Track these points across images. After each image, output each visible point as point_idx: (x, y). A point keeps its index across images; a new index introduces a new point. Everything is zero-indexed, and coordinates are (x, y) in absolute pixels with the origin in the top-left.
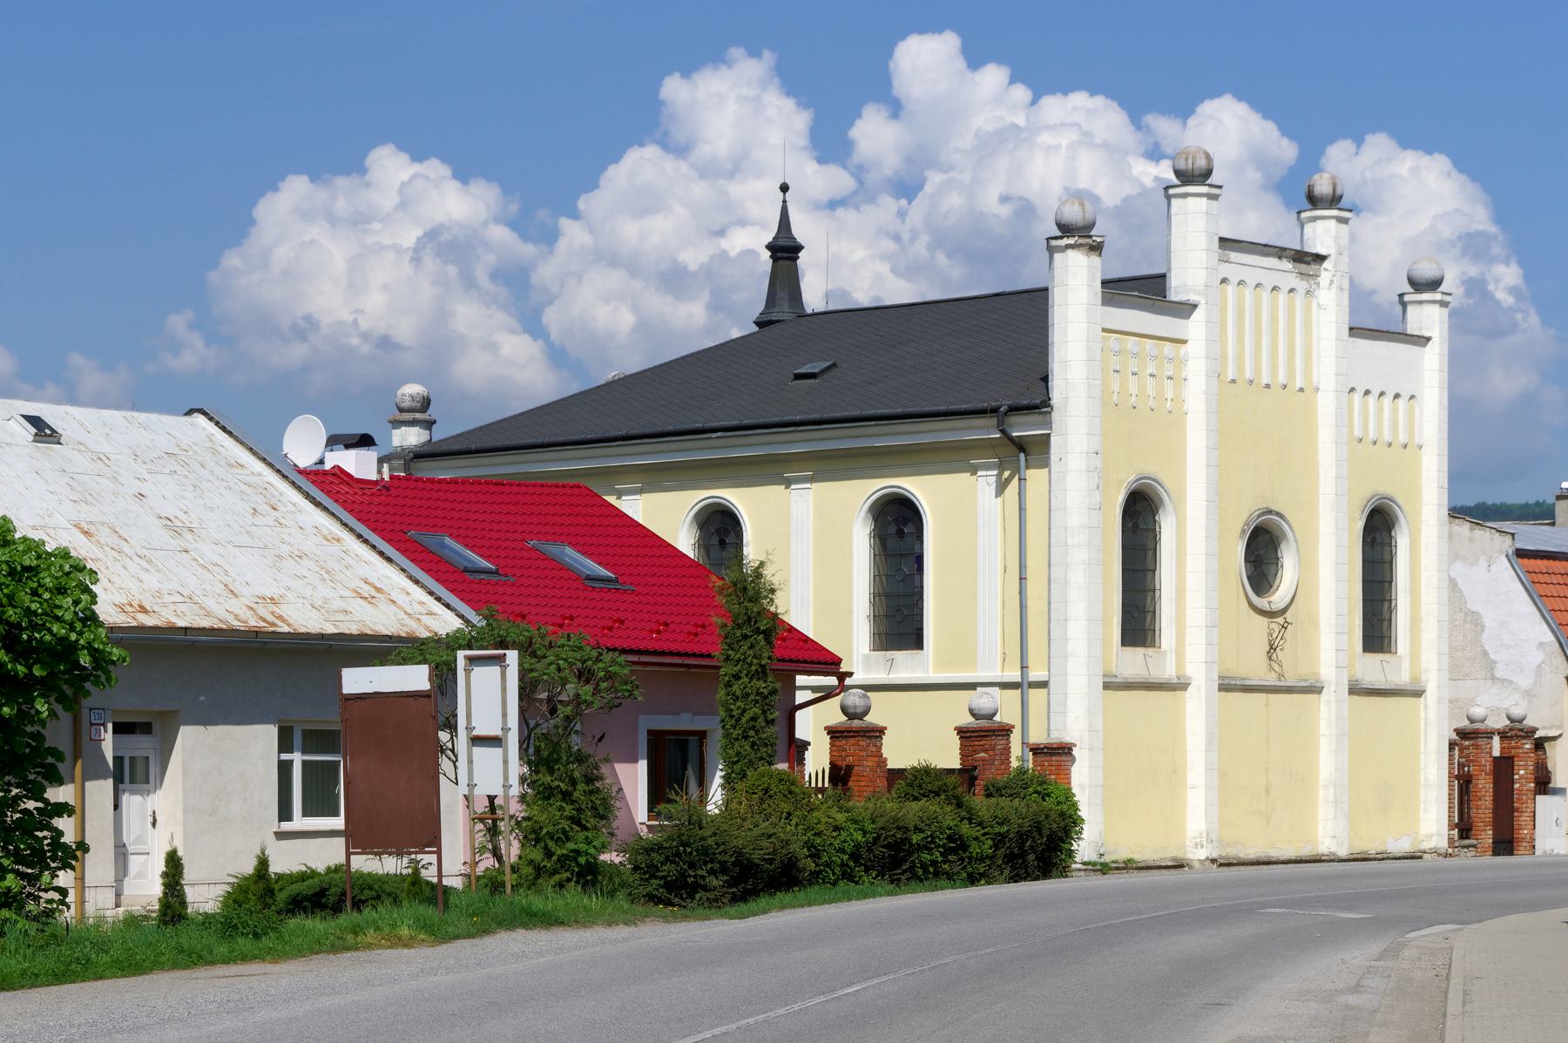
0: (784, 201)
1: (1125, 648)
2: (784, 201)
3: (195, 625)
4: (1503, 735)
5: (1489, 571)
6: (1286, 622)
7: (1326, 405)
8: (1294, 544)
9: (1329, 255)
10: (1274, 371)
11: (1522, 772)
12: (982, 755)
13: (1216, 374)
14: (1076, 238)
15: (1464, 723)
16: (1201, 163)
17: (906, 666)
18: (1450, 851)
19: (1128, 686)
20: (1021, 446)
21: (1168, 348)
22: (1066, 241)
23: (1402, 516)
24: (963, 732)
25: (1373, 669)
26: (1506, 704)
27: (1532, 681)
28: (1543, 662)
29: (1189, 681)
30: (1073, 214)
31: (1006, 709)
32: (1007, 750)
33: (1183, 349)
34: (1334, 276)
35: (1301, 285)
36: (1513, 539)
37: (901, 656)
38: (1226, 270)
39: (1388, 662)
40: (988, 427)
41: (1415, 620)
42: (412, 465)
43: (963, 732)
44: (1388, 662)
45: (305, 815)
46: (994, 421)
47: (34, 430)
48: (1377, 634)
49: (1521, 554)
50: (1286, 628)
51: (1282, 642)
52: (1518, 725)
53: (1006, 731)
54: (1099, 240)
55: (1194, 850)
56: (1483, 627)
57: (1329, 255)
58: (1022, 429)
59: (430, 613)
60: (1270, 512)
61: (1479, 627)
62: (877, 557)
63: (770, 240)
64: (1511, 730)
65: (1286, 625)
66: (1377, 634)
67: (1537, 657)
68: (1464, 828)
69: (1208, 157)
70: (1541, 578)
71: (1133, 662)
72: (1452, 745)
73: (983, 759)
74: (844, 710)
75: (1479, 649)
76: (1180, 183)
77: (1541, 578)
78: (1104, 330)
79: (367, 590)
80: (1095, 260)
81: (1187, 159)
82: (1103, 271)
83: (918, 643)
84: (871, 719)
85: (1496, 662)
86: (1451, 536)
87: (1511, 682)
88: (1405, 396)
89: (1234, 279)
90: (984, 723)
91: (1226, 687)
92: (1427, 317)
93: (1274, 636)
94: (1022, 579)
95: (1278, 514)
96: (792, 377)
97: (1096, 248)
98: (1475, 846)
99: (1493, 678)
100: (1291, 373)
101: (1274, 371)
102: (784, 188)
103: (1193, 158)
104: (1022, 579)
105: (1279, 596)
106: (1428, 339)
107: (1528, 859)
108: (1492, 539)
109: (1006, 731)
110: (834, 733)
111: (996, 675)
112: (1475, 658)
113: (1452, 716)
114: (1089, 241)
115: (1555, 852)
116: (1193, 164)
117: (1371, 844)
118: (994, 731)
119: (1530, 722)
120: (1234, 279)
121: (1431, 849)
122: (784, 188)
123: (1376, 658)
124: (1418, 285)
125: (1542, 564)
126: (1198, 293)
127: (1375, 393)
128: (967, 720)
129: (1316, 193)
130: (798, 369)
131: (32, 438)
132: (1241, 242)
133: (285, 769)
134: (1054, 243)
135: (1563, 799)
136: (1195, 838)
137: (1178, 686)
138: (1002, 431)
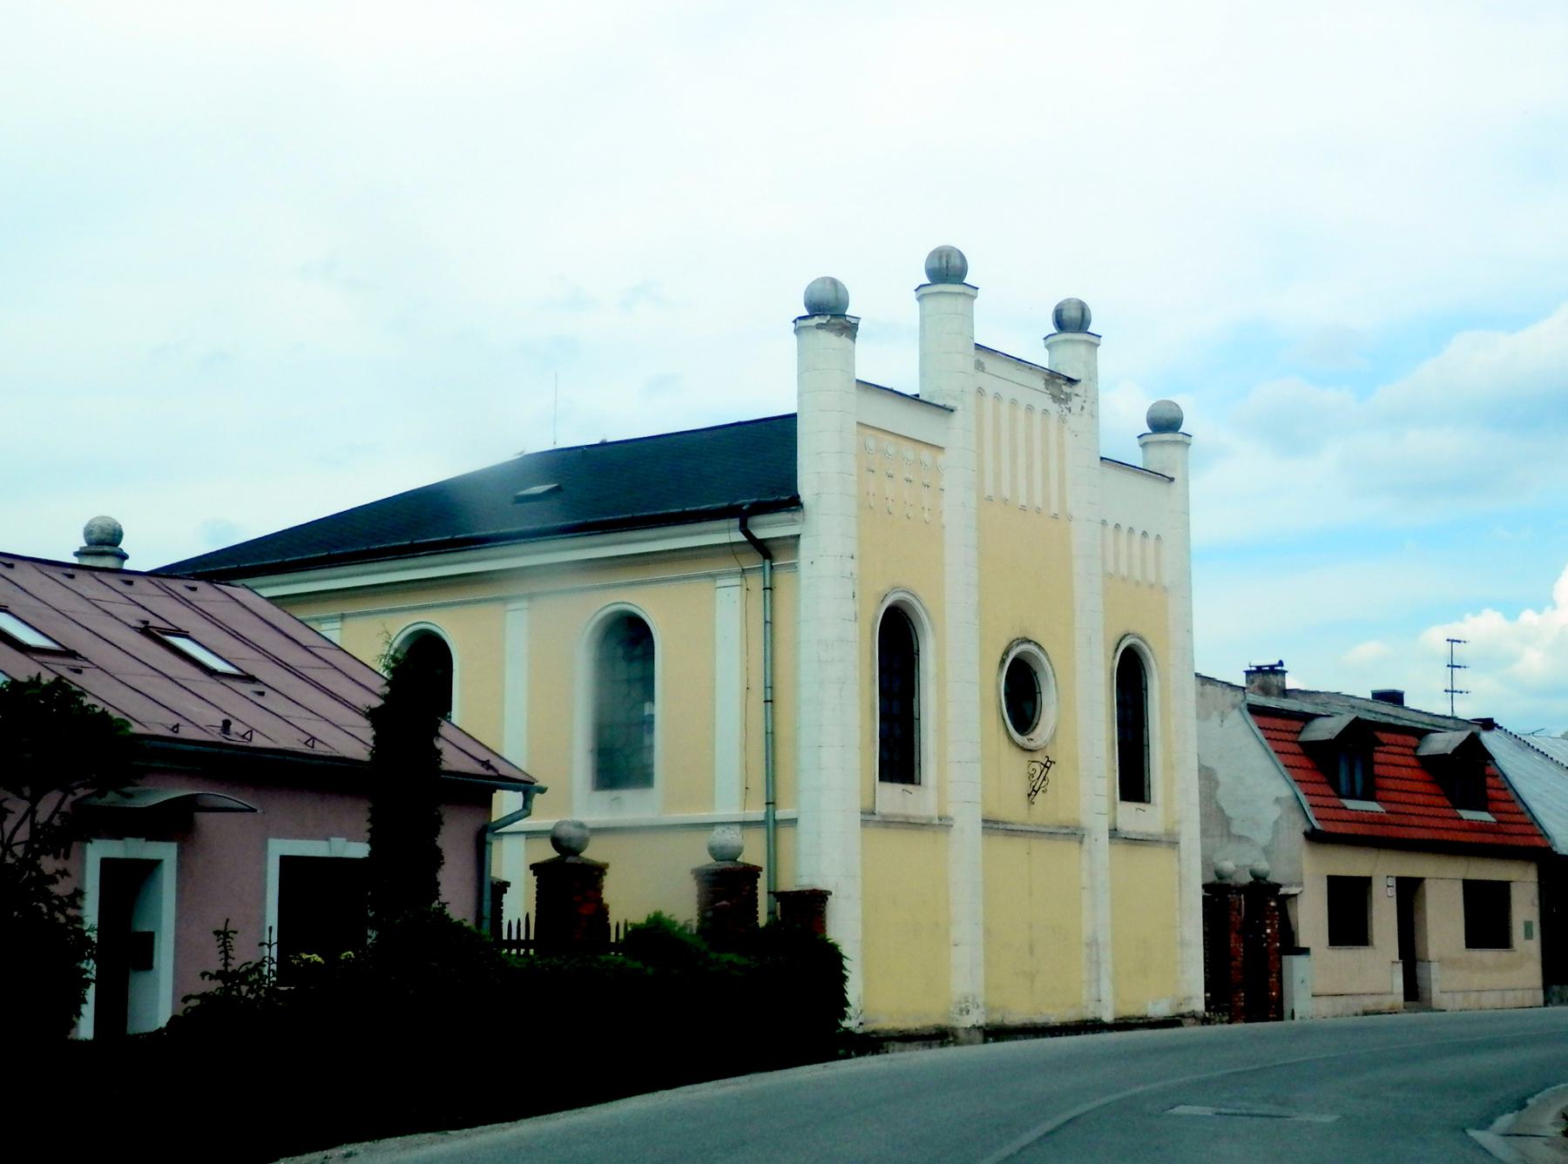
5: (1221, 726)
6: (1048, 761)
8: (1053, 678)
9: (1080, 381)
11: (1268, 931)
14: (829, 317)
15: (1212, 878)
17: (631, 807)
18: (1207, 1014)
20: (764, 549)
21: (926, 454)
22: (817, 320)
23: (1152, 659)
25: (1132, 817)
26: (1247, 861)
27: (1270, 837)
28: (1280, 817)
29: (951, 823)
31: (753, 853)
33: (941, 458)
34: (1085, 402)
35: (1054, 408)
36: (1244, 694)
38: (983, 380)
39: (1144, 811)
40: (729, 530)
44: (1144, 811)
45: (1332, 881)
46: (736, 522)
48: (1134, 784)
50: (1049, 768)
51: (1045, 783)
54: (853, 321)
55: (958, 1016)
56: (1217, 783)
57: (1080, 381)
58: (768, 528)
61: (1213, 784)
62: (581, 450)
65: (1048, 764)
66: (1134, 784)
67: (1273, 813)
71: (893, 796)
75: (1214, 806)
76: (929, 282)
78: (859, 424)
85: (1081, 842)
87: (1248, 839)
90: (728, 865)
91: (991, 825)
93: (1036, 776)
94: (769, 701)
99: (1229, 835)
103: (947, 256)
108: (1223, 694)
109: (752, 873)
112: (1211, 815)
116: (947, 262)
120: (990, 392)
121: (1189, 1013)
123: (1131, 807)
125: (1279, 723)
126: (955, 398)
128: (706, 860)
129: (1064, 317)
132: (997, 351)
134: (804, 323)
135: (1307, 959)
136: (960, 1003)
137: (942, 824)
138: (746, 533)
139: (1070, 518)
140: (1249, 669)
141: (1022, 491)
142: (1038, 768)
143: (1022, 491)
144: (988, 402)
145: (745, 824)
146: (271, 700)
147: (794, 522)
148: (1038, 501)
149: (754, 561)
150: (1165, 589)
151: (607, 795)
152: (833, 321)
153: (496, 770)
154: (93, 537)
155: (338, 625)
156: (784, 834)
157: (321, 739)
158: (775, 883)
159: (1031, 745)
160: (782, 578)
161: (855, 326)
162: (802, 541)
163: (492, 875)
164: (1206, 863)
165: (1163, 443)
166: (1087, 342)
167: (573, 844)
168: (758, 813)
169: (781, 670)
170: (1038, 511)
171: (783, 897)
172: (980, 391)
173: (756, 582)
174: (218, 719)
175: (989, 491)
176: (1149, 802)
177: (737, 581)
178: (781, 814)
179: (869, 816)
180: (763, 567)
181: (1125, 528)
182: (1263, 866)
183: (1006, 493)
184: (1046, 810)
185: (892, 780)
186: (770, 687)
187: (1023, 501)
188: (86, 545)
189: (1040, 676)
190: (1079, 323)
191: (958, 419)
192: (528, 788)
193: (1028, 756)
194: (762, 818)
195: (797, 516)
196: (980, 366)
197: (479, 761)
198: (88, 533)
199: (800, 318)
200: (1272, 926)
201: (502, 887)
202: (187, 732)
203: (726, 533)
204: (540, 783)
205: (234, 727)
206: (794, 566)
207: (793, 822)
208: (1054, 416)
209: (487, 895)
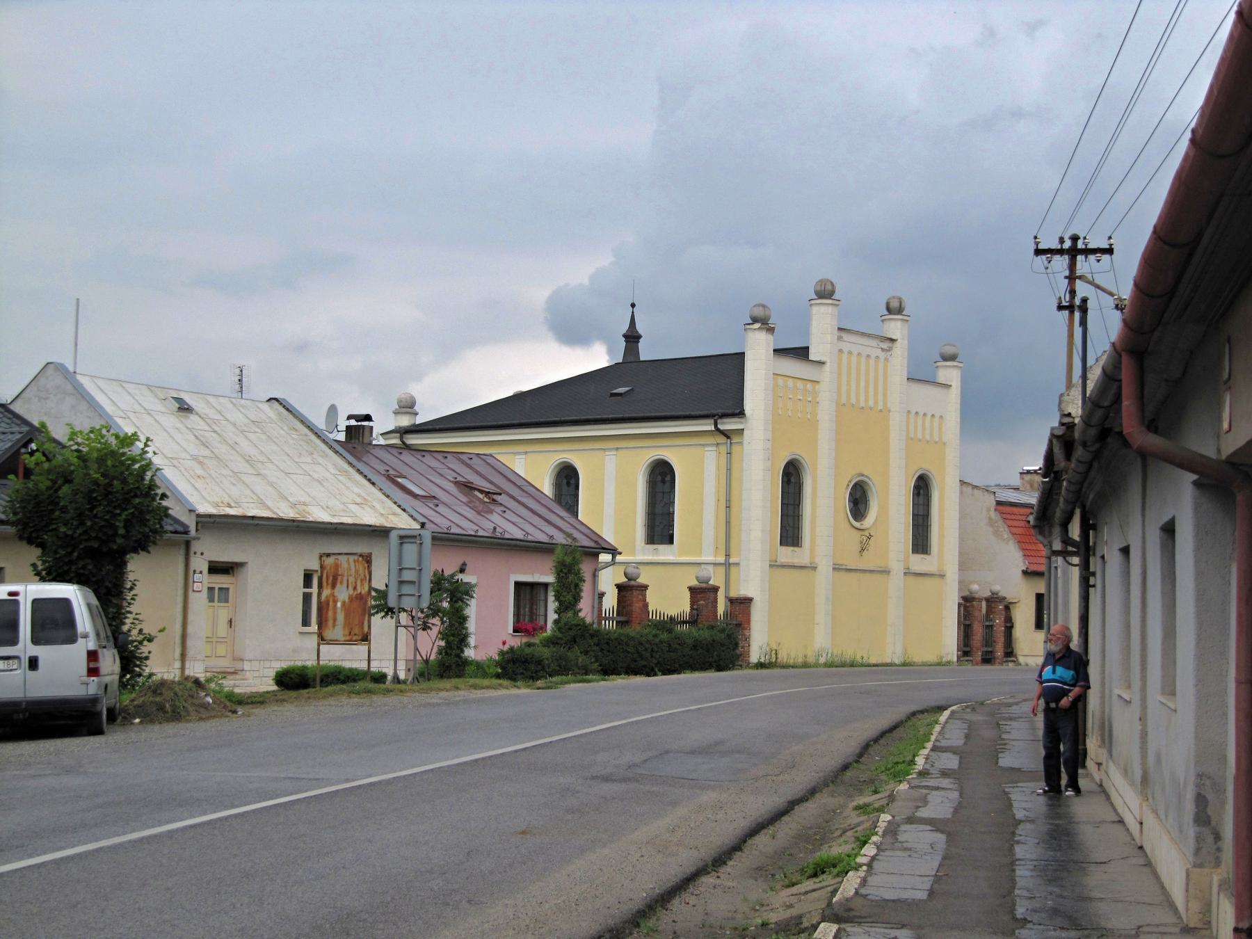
0: (633, 312)
1: (782, 547)
2: (633, 312)
3: (258, 515)
4: (987, 600)
7: (896, 420)
10: (867, 401)
11: (997, 621)
12: (702, 602)
13: (840, 406)
15: (966, 593)
16: (829, 287)
17: (664, 553)
19: (783, 566)
20: (726, 434)
21: (809, 386)
24: (692, 590)
25: (919, 563)
30: (759, 312)
31: (717, 579)
32: (715, 601)
35: (882, 355)
37: (661, 547)
38: (844, 346)
41: (941, 536)
42: (404, 436)
43: (692, 590)
47: (177, 405)
48: (921, 543)
49: (999, 503)
52: (995, 596)
53: (715, 589)
54: (772, 326)
58: (728, 425)
59: (394, 514)
60: (863, 475)
63: (625, 332)
64: (992, 598)
66: (921, 543)
68: (965, 651)
69: (832, 284)
70: (1008, 516)
71: (787, 554)
72: (960, 605)
73: (702, 605)
74: (626, 575)
77: (1008, 516)
78: (774, 374)
79: (359, 500)
80: (770, 337)
81: (821, 285)
82: (774, 345)
83: (671, 541)
84: (641, 580)
86: (961, 492)
88: (937, 416)
89: (855, 352)
90: (704, 585)
91: (837, 568)
92: (950, 374)
94: (728, 507)
95: (866, 476)
96: (609, 394)
97: (771, 330)
98: (971, 660)
100: (876, 402)
101: (867, 401)
102: (633, 305)
104: (728, 507)
105: (868, 521)
106: (951, 386)
107: (1006, 667)
109: (715, 589)
110: (620, 587)
111: (711, 559)
113: (960, 590)
114: (766, 326)
115: (944, 660)
117: (850, 651)
118: (708, 589)
119: (1002, 594)
120: (846, 350)
122: (633, 305)
123: (918, 557)
124: (946, 358)
125: (1009, 509)
127: (921, 414)
128: (694, 583)
130: (616, 389)
131: (177, 410)
133: (307, 598)
134: (748, 327)
139: (889, 411)
140: (1022, 471)
141: (862, 399)
142: (865, 538)
143: (862, 399)
144: (845, 356)
145: (715, 564)
146: (508, 515)
147: (741, 423)
148: (871, 403)
149: (722, 439)
150: (945, 444)
151: (652, 547)
152: (763, 326)
153: (600, 545)
154: (402, 404)
155: (524, 457)
156: (733, 569)
157: (532, 534)
158: (729, 593)
159: (862, 527)
160: (735, 449)
161: (773, 328)
162: (745, 432)
163: (599, 588)
164: (961, 583)
165: (947, 366)
166: (902, 320)
167: (634, 576)
168: (721, 559)
169: (735, 492)
170: (871, 409)
171: (732, 601)
172: (841, 351)
173: (723, 449)
174: (491, 526)
175: (844, 400)
176: (930, 554)
177: (714, 448)
178: (732, 560)
179: (774, 565)
180: (727, 443)
181: (921, 414)
182: (996, 588)
183: (853, 401)
184: (869, 561)
185: (787, 545)
186: (728, 500)
187: (862, 404)
188: (398, 408)
189: (869, 494)
190: (898, 309)
191: (827, 367)
192: (614, 552)
193: (861, 533)
194: (723, 562)
195: (742, 420)
196: (840, 338)
197: (594, 541)
198: (399, 402)
199: (747, 324)
200: (1000, 619)
201: (602, 595)
202: (481, 533)
203: (708, 426)
204: (620, 550)
205: (498, 529)
206: (741, 443)
207: (738, 564)
208: (882, 359)
209: (596, 597)
